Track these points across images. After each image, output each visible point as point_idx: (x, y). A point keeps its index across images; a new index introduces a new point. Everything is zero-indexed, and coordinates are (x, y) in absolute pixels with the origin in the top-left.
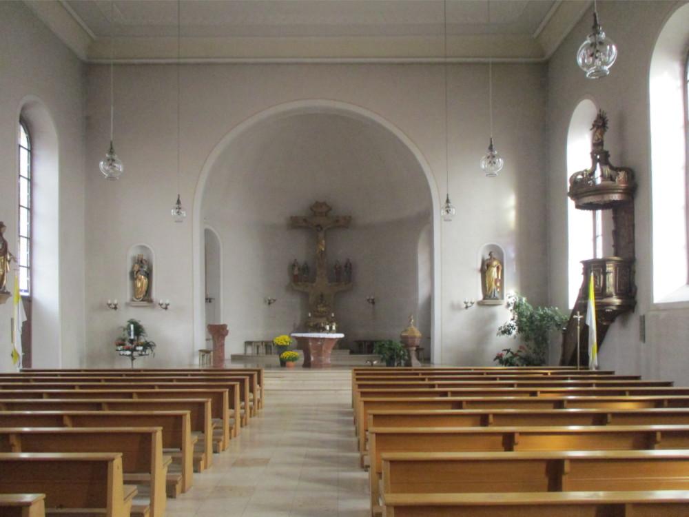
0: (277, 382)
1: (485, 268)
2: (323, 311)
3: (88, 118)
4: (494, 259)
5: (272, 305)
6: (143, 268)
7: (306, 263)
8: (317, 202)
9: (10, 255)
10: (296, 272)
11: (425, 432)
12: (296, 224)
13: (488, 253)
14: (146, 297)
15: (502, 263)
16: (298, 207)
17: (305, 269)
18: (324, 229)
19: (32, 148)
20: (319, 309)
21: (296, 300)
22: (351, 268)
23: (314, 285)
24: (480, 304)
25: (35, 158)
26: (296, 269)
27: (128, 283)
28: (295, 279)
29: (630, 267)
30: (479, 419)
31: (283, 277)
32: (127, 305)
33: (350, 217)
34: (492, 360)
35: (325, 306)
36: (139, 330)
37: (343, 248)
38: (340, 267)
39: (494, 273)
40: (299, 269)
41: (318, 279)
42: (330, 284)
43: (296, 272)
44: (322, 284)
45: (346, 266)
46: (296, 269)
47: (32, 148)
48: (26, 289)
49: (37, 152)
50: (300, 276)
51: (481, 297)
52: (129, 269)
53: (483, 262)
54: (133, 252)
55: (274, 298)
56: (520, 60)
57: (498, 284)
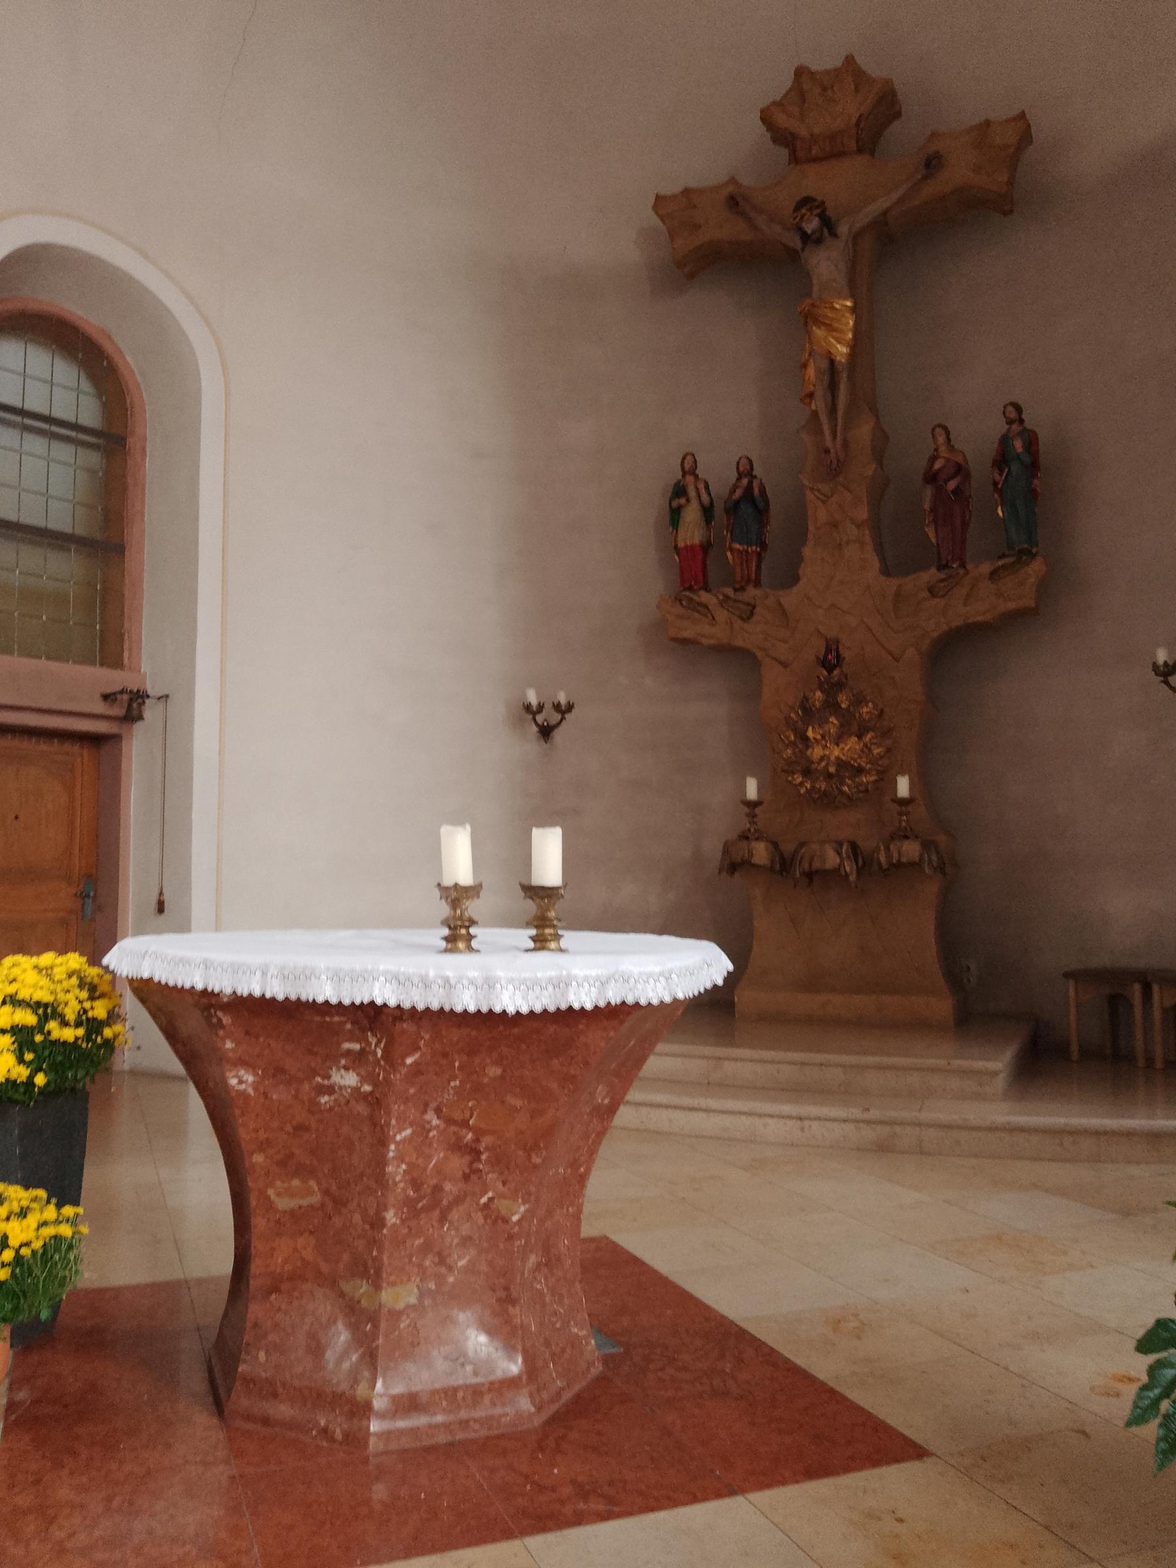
0: (941, 1116)
2: (841, 764)
5: (558, 735)
7: (746, 471)
10: (692, 531)
12: (721, 246)
13: (138, 727)
16: (719, 144)
17: (747, 507)
18: (843, 229)
20: (817, 752)
21: (706, 710)
22: (1034, 467)
23: (790, 599)
26: (692, 514)
28: (692, 572)
31: (626, 570)
34: (1121, 1423)
35: (851, 726)
37: (992, 350)
38: (960, 470)
40: (708, 512)
41: (814, 562)
42: (893, 583)
43: (692, 531)
44: (841, 588)
45: (1002, 459)
46: (692, 514)
50: (722, 547)
55: (562, 698)
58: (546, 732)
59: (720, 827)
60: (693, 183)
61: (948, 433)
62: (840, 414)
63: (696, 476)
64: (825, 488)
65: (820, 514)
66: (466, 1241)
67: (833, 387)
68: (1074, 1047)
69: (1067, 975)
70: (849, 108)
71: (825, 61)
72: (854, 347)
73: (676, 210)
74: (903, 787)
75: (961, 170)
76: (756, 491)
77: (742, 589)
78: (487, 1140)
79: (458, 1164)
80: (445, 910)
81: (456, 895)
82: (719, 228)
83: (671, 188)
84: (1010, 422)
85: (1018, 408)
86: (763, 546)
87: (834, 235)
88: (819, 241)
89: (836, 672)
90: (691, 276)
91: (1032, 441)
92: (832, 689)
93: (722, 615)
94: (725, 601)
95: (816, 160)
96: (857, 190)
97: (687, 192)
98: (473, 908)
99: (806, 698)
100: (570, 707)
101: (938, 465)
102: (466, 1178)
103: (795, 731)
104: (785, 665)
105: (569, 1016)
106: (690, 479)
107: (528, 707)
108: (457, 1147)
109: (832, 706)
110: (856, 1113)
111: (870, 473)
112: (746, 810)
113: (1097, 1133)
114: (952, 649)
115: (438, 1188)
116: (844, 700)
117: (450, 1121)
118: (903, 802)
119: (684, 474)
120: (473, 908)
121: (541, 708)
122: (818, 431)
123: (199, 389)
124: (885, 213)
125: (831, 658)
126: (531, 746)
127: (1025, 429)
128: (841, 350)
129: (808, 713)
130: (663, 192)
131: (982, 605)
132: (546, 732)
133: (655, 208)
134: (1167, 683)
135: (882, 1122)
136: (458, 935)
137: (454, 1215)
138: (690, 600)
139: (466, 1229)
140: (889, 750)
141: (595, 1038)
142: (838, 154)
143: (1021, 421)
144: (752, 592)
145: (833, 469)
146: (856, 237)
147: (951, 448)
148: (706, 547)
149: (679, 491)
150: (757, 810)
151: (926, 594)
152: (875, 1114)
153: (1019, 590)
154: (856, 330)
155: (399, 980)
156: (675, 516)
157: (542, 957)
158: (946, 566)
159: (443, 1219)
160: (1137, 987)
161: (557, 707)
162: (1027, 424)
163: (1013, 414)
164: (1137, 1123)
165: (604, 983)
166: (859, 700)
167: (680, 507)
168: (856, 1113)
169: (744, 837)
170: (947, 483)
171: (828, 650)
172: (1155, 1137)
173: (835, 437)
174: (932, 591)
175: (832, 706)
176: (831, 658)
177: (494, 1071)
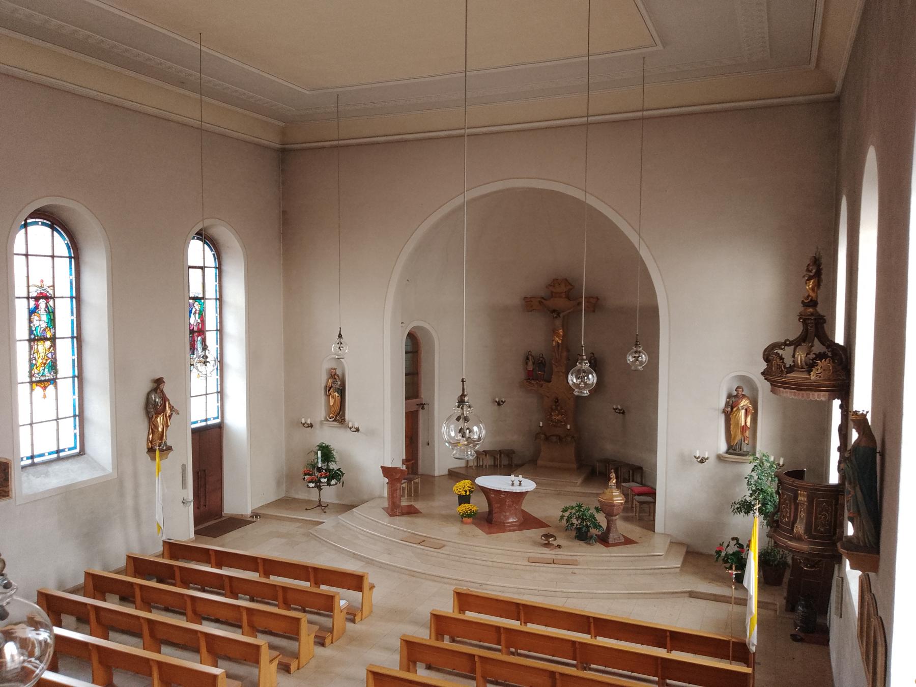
1: (730, 410)
3: (284, 212)
4: (744, 396)
6: (337, 387)
8: (327, 447)
9: (172, 408)
10: (530, 368)
11: (554, 635)
12: (531, 304)
14: (338, 415)
15: (755, 403)
18: (561, 315)
19: (220, 264)
24: (720, 458)
25: (224, 274)
26: (530, 363)
27: (323, 398)
29: (837, 500)
30: (687, 595)
32: (321, 423)
35: (560, 413)
36: (327, 453)
39: (743, 418)
40: (534, 363)
43: (530, 368)
46: (530, 363)
47: (220, 264)
48: (216, 415)
49: (225, 268)
51: (723, 447)
52: (323, 385)
53: (730, 396)
54: (327, 365)
56: (801, 99)
57: (747, 434)
70: (563, 288)
74: (569, 427)
92: (556, 406)
126: (496, 407)
132: (499, 404)
149: (528, 359)
176: (556, 401)
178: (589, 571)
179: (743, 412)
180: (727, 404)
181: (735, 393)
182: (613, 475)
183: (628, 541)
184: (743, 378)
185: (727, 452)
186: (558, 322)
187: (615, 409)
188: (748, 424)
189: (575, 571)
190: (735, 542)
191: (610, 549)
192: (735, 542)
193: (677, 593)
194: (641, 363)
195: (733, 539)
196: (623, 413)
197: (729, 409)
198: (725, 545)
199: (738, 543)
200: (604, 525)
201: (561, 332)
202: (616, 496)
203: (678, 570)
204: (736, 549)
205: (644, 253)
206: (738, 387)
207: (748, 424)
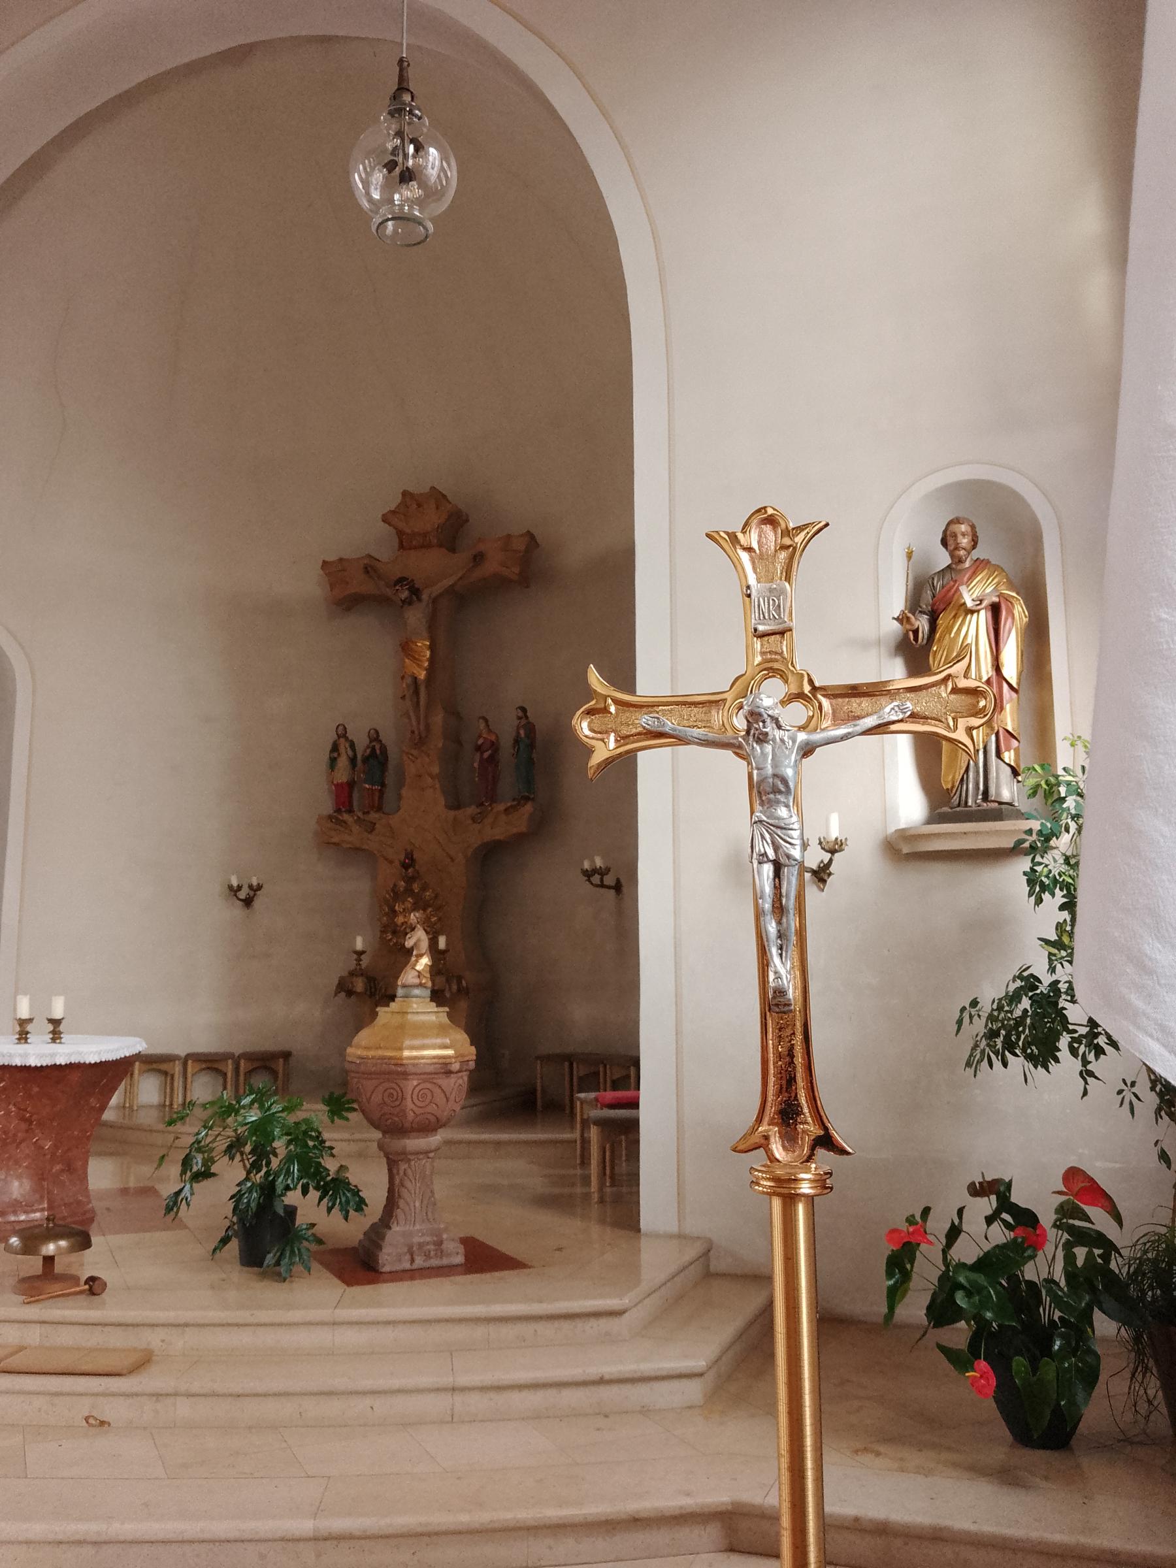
4: (980, 565)
5: (257, 903)
7: (375, 737)
10: (342, 774)
16: (362, 533)
17: (375, 760)
18: (425, 597)
24: (903, 850)
26: (343, 762)
28: (344, 796)
30: (712, 1533)
33: (531, 536)
38: (495, 746)
40: (353, 761)
42: (452, 813)
44: (422, 814)
45: (517, 741)
46: (343, 762)
51: (909, 806)
58: (248, 902)
59: (341, 966)
60: (348, 554)
61: (486, 721)
62: (422, 708)
63: (347, 739)
64: (415, 752)
65: (411, 769)
66: (28, 1156)
67: (416, 692)
68: (539, 1102)
69: (538, 1058)
70: (431, 520)
71: (419, 487)
72: (431, 671)
73: (335, 571)
75: (491, 566)
76: (378, 752)
77: (368, 813)
78: (35, 1117)
79: (24, 1126)
80: (18, 1029)
81: (23, 1023)
82: (359, 584)
83: (331, 558)
84: (519, 718)
85: (524, 710)
86: (383, 785)
87: (419, 600)
88: (410, 603)
89: (410, 870)
90: (348, 609)
91: (530, 729)
92: (410, 880)
93: (356, 829)
94: (359, 821)
95: (415, 548)
96: (435, 568)
97: (341, 560)
98: (29, 1028)
99: (395, 885)
100: (260, 887)
101: (480, 742)
102: (27, 1131)
103: (389, 906)
104: (391, 862)
105: (56, 1067)
106: (342, 740)
107: (231, 887)
108: (23, 1119)
109: (409, 891)
110: (346, 1136)
111: (440, 745)
112: (355, 956)
113: (469, 1143)
114: (490, 855)
115: (15, 1135)
116: (416, 887)
117: (20, 1109)
118: (443, 952)
119: (339, 736)
120: (29, 1028)
121: (240, 888)
122: (409, 718)
123: (15, 691)
124: (452, 586)
125: (409, 862)
126: (238, 910)
127: (529, 723)
128: (422, 675)
129: (396, 895)
130: (327, 559)
131: (498, 828)
132: (248, 902)
133: (323, 567)
134: (589, 880)
135: (360, 1140)
136: (23, 1037)
137: (23, 1145)
138: (337, 819)
139: (27, 1151)
140: (440, 919)
141: (75, 1077)
142: (429, 546)
143: (527, 717)
144: (373, 816)
145: (420, 741)
146: (435, 601)
147: (490, 731)
148: (351, 785)
149: (335, 748)
150: (363, 957)
151: (470, 821)
152: (357, 1136)
153: (520, 821)
154: (432, 660)
155: (41, 1056)
156: (333, 762)
157: (53, 1045)
158: (482, 804)
159: (17, 1147)
160: (567, 1064)
161: (251, 887)
162: (530, 720)
163: (520, 714)
164: (485, 1137)
165: (70, 1055)
166: (424, 888)
167: (335, 759)
168: (346, 1136)
169: (352, 974)
170: (490, 754)
171: (406, 857)
172: (498, 1144)
173: (419, 723)
174: (474, 820)
175: (409, 891)
176: (409, 862)
177: (36, 1089)
178: (183, 1409)
179: (976, 628)
180: (914, 604)
181: (943, 559)
182: (418, 938)
183: (482, 1259)
184: (978, 492)
185: (930, 820)
186: (415, 617)
187: (588, 874)
188: (1011, 670)
189: (111, 1410)
190: (988, 1204)
191: (386, 1289)
192: (988, 1204)
193: (636, 1522)
194: (431, 194)
195: (978, 1190)
196: (618, 887)
197: (922, 623)
198: (938, 1226)
199: (1005, 1205)
200: (371, 1181)
201: (423, 646)
202: (421, 1031)
203: (693, 1391)
204: (999, 1235)
205: (565, 97)
206: (957, 521)
207: (1011, 670)
